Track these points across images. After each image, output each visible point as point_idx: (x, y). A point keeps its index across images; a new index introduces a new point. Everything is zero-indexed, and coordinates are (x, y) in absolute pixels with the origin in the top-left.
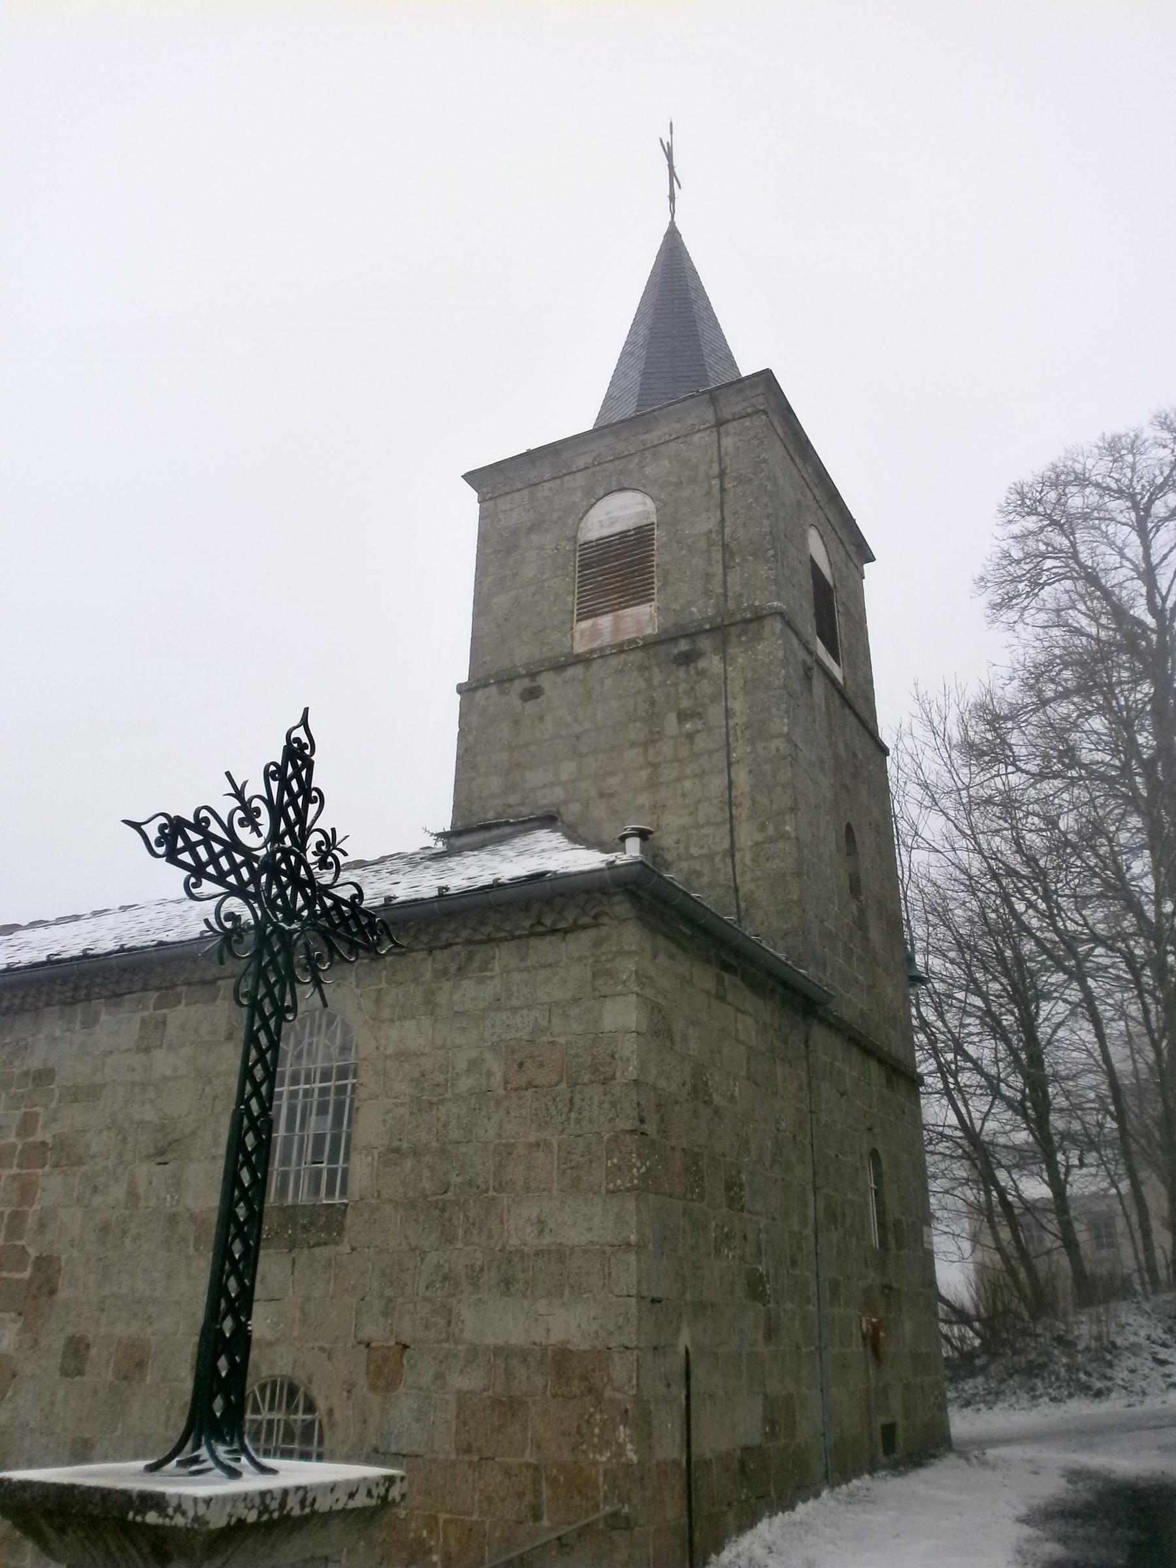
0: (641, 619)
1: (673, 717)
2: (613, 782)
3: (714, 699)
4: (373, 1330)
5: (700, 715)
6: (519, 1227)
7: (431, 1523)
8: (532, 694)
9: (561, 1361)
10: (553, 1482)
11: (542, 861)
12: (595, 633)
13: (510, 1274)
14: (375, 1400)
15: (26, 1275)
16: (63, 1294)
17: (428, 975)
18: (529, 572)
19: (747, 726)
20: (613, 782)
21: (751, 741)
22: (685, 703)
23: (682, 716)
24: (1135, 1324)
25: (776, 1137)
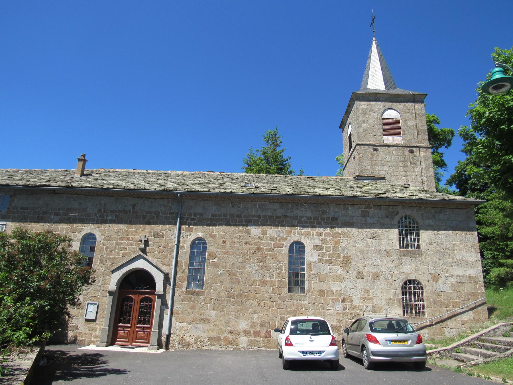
0: (398, 140)
1: (409, 162)
2: (397, 173)
3: (418, 161)
4: (433, 272)
5: (415, 164)
6: (459, 256)
7: (449, 301)
8: (376, 150)
9: (470, 277)
10: (471, 295)
11: (311, 183)
12: (388, 140)
13: (458, 264)
14: (434, 283)
15: (342, 259)
16: (353, 263)
17: (433, 212)
18: (371, 121)
19: (425, 168)
20: (397, 173)
21: (426, 171)
22: (411, 160)
23: (411, 163)
24: (510, 283)
25: (65, 272)
